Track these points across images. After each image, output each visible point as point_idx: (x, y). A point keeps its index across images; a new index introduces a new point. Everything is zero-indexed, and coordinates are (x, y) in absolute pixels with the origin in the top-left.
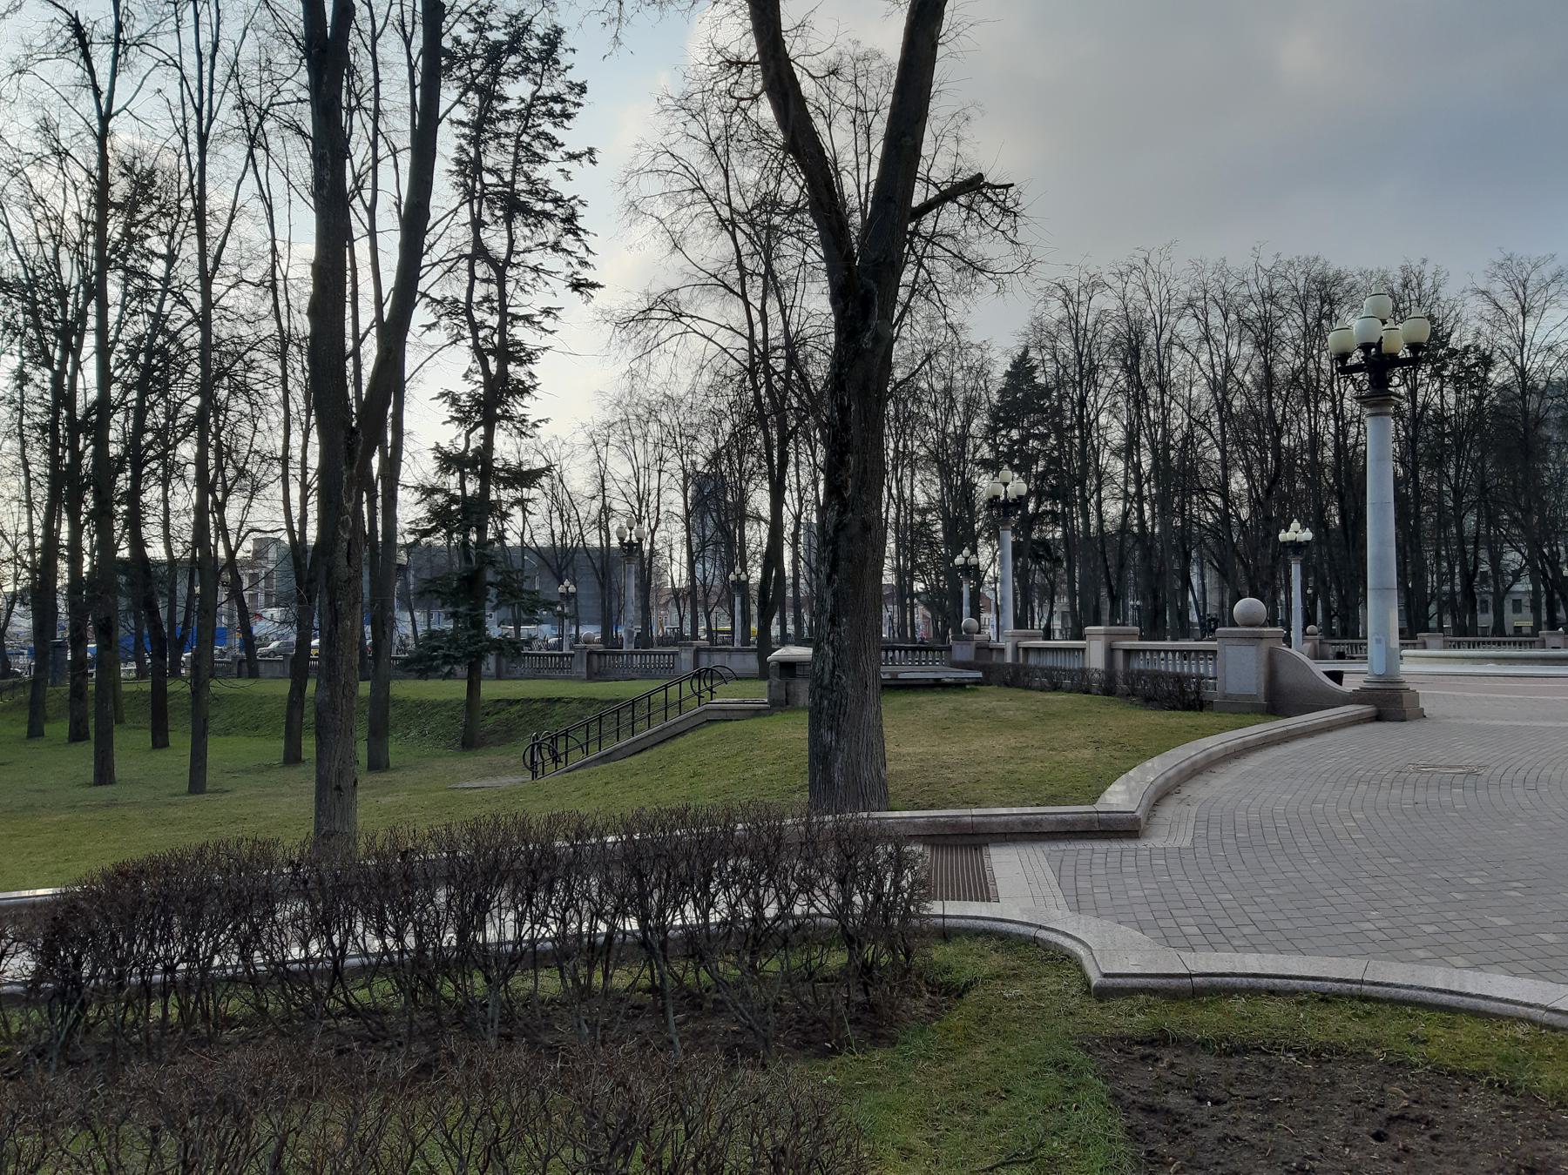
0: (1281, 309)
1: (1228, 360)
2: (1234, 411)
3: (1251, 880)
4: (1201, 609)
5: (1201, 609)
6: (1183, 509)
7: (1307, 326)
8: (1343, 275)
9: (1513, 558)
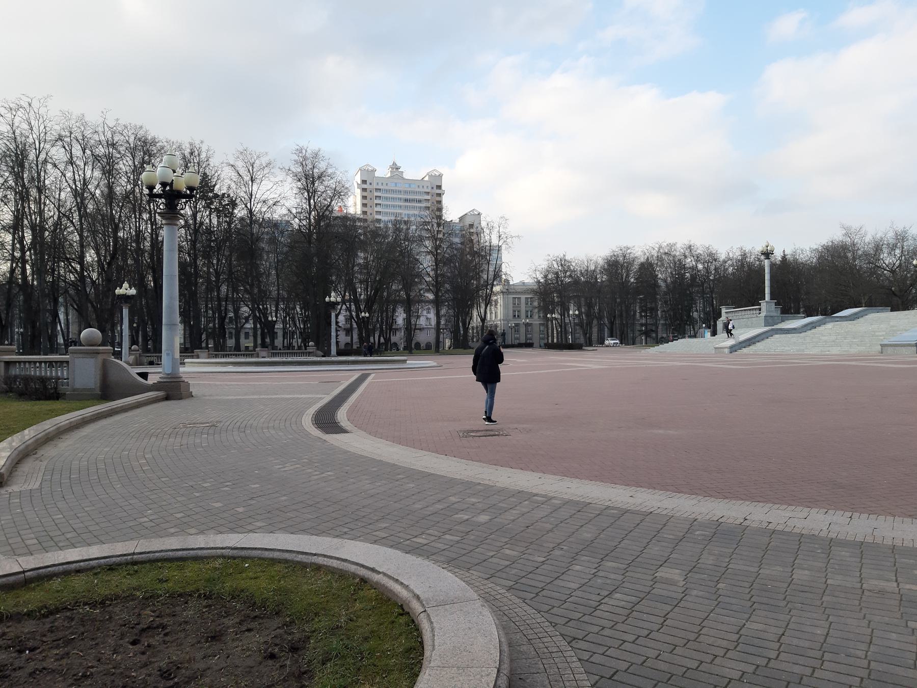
0: (119, 153)
1: (84, 180)
2: (88, 211)
3: (77, 503)
4: (66, 335)
5: (66, 335)
6: (53, 270)
7: (135, 166)
8: (157, 140)
9: (245, 310)
